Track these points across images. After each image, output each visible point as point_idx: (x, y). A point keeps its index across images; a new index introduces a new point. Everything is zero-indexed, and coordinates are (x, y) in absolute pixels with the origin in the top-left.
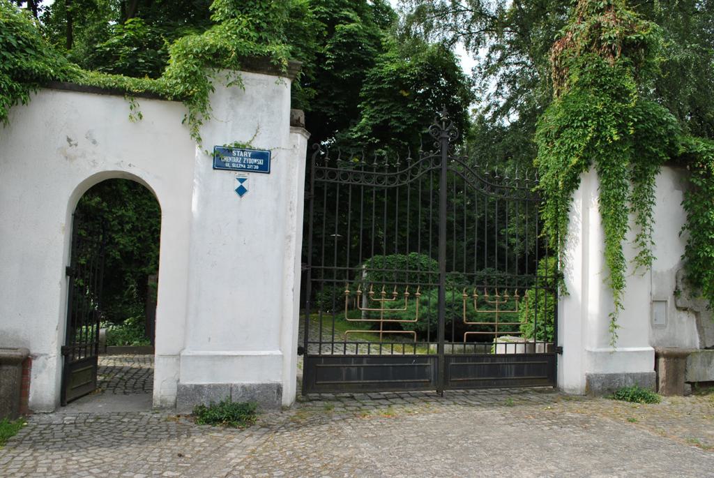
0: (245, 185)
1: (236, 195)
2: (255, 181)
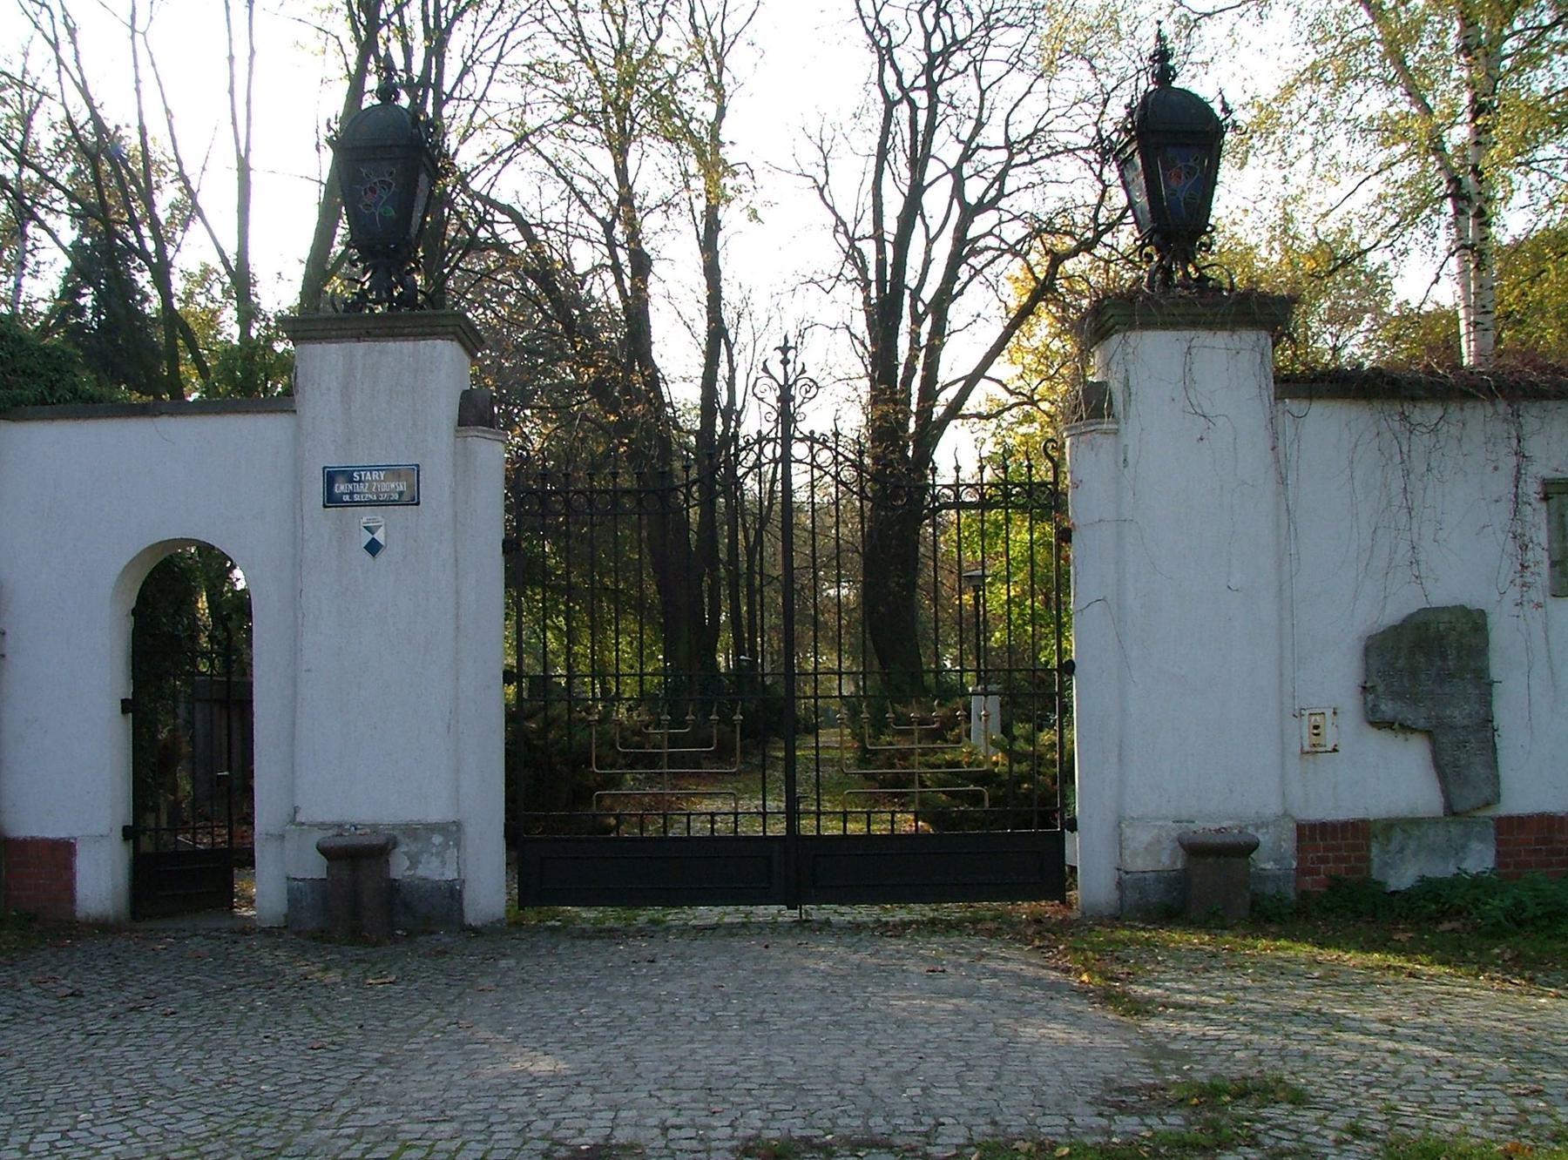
0: (380, 536)
1: (368, 556)
2: (385, 525)
